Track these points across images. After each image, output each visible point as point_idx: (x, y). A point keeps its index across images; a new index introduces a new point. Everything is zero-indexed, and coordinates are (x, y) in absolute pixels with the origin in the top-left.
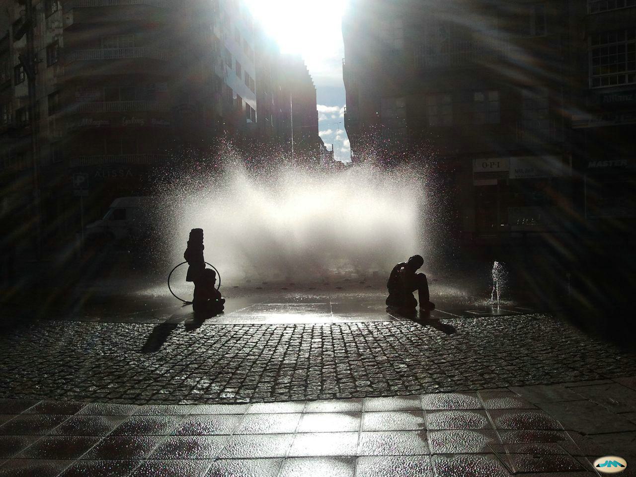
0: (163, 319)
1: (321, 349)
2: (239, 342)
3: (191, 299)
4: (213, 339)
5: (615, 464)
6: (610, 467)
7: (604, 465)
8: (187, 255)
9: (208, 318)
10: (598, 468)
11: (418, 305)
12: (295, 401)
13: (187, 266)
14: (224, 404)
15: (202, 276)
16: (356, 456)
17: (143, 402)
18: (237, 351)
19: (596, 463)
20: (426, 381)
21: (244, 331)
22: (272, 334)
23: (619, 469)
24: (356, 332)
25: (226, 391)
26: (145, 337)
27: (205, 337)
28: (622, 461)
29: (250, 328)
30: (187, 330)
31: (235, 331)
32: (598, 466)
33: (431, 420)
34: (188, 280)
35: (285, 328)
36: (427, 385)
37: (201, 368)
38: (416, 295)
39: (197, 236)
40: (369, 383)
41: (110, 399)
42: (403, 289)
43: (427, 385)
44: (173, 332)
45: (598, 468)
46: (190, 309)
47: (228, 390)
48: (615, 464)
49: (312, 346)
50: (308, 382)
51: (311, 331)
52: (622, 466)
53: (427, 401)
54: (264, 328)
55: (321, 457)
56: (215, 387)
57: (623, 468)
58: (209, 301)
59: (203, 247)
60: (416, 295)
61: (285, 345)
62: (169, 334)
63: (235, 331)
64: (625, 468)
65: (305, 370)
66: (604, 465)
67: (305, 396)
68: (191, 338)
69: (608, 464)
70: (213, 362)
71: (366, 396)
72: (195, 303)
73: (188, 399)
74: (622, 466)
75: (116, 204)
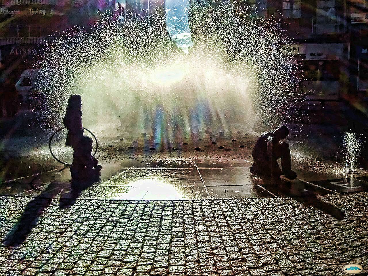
0: (39, 190)
2: (115, 229)
3: (71, 163)
4: (87, 223)
5: (356, 268)
7: (350, 269)
8: (66, 122)
9: (85, 188)
15: (80, 143)
18: (113, 245)
21: (121, 212)
22: (151, 216)
23: (357, 272)
26: (14, 218)
27: (78, 220)
29: (126, 207)
30: (61, 208)
31: (110, 211)
32: (346, 270)
34: (67, 145)
35: (164, 207)
39: (75, 102)
44: (45, 211)
45: (346, 271)
46: (68, 175)
48: (356, 268)
51: (190, 212)
52: (360, 270)
54: (141, 206)
58: (85, 173)
59: (80, 113)
61: (167, 235)
62: (40, 215)
63: (110, 211)
66: (350, 269)
68: (63, 221)
69: (352, 268)
70: (84, 267)
74: (360, 270)
75: (26, 73)
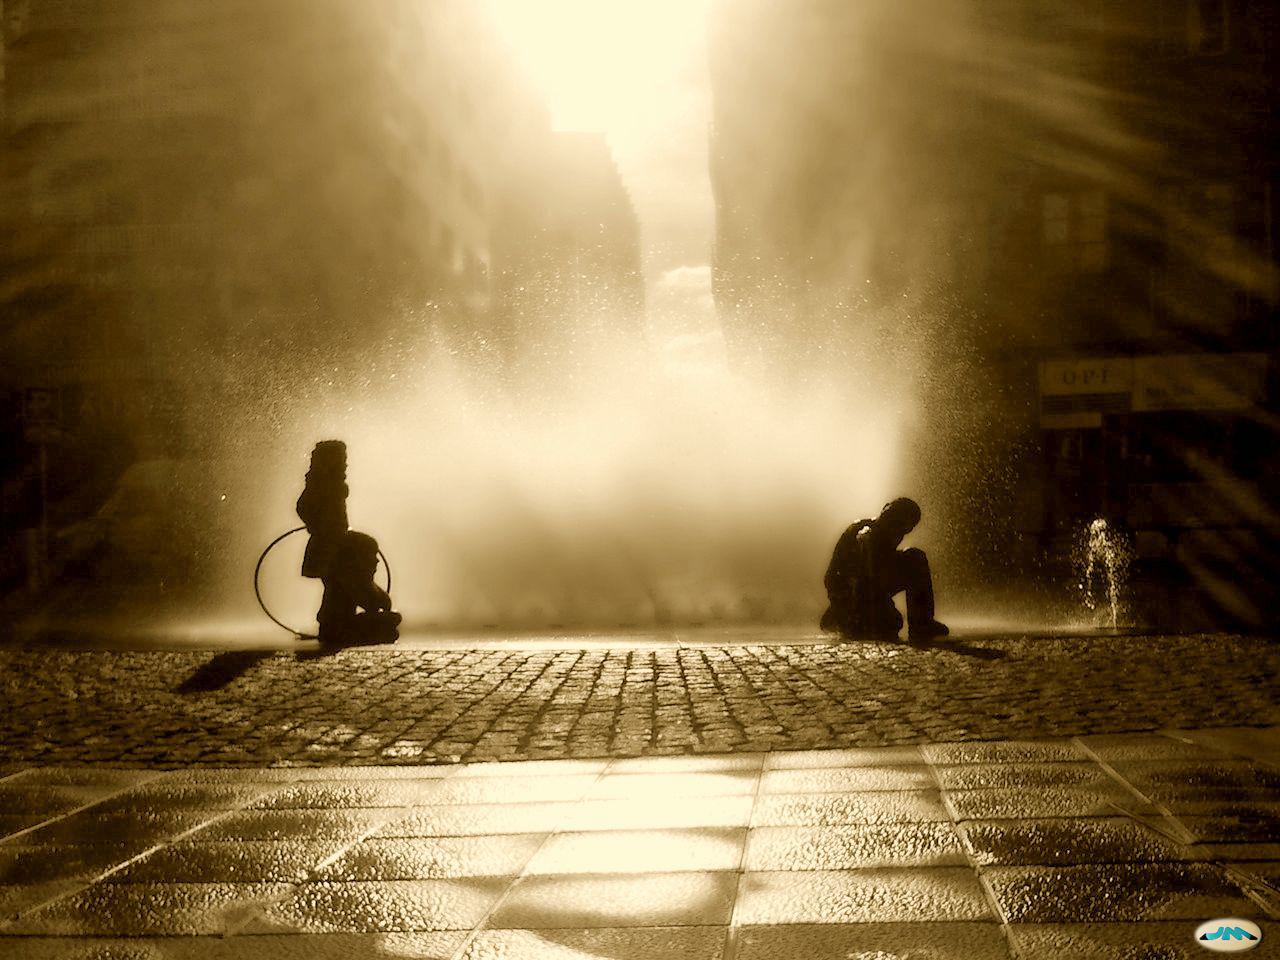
1: (651, 684)
5: (1238, 933)
6: (1228, 939)
7: (1216, 935)
10: (1203, 942)
11: (906, 623)
12: (583, 758)
13: (304, 537)
14: (394, 765)
15: (343, 561)
16: (747, 828)
17: (175, 765)
19: (1199, 932)
20: (934, 725)
23: (1245, 944)
24: (745, 659)
25: (397, 744)
28: (1252, 928)
32: (1204, 938)
33: (943, 777)
36: (933, 731)
37: (335, 711)
38: (900, 601)
39: (329, 463)
40: (780, 729)
41: (87, 762)
42: (870, 579)
43: (933, 731)
45: (1203, 942)
47: (403, 743)
48: (1238, 933)
49: (628, 679)
50: (618, 730)
52: (1253, 938)
53: (930, 754)
55: (660, 830)
56: (368, 740)
57: (1254, 943)
59: (344, 491)
60: (900, 601)
64: (1258, 940)
65: (610, 713)
66: (1216, 935)
67: (608, 750)
69: (1225, 934)
71: (772, 749)
72: (320, 638)
73: (296, 760)
74: (1253, 938)
